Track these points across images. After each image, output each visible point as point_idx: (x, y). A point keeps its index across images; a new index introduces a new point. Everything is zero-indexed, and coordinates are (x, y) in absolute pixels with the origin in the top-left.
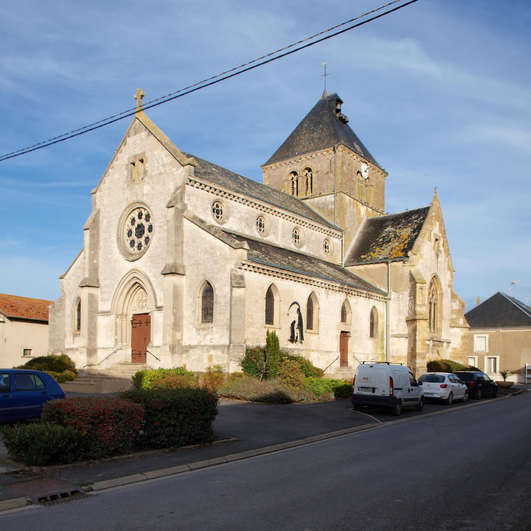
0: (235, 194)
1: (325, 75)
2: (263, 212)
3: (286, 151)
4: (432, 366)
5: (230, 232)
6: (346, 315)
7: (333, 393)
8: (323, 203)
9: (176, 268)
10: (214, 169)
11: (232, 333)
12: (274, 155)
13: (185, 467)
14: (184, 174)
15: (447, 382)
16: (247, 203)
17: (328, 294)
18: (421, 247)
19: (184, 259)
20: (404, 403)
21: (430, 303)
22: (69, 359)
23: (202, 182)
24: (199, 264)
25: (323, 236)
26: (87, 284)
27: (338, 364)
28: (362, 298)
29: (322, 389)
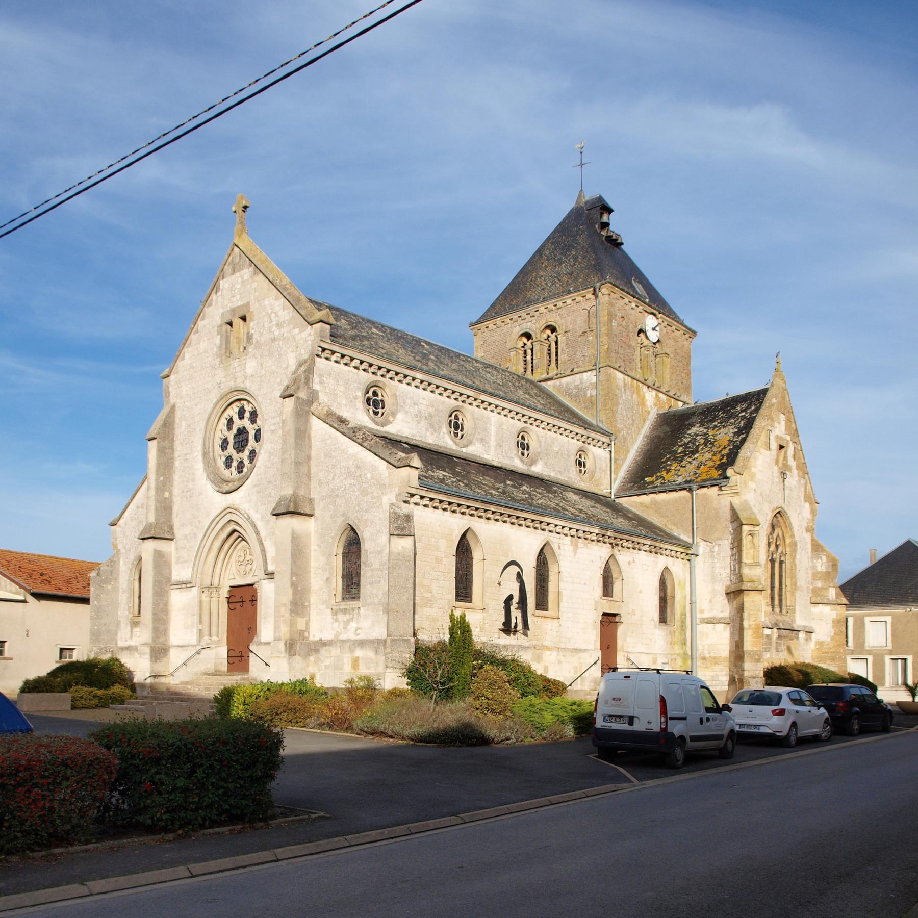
0: (408, 372)
1: (582, 165)
2: (461, 404)
3: (515, 296)
4: (775, 675)
5: (399, 438)
6: (612, 583)
7: (571, 726)
8: (577, 387)
9: (296, 504)
10: (374, 330)
11: (390, 617)
12: (493, 306)
13: (182, 871)
14: (312, 338)
15: (785, 704)
16: (430, 388)
17: (576, 547)
18: (752, 460)
19: (312, 487)
20: (690, 744)
21: (772, 561)
22: (122, 665)
23: (345, 352)
24: (337, 496)
25: (575, 444)
26: (152, 534)
27: (596, 671)
28: (642, 553)
29: (548, 718)
